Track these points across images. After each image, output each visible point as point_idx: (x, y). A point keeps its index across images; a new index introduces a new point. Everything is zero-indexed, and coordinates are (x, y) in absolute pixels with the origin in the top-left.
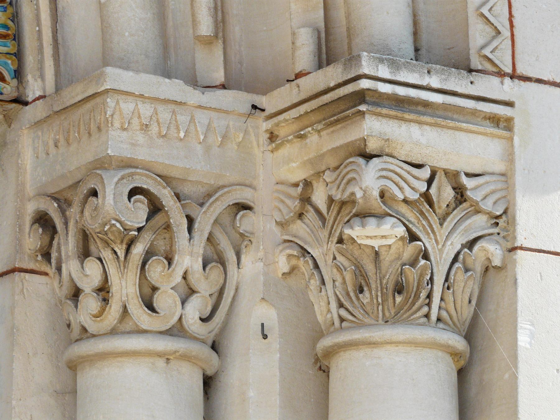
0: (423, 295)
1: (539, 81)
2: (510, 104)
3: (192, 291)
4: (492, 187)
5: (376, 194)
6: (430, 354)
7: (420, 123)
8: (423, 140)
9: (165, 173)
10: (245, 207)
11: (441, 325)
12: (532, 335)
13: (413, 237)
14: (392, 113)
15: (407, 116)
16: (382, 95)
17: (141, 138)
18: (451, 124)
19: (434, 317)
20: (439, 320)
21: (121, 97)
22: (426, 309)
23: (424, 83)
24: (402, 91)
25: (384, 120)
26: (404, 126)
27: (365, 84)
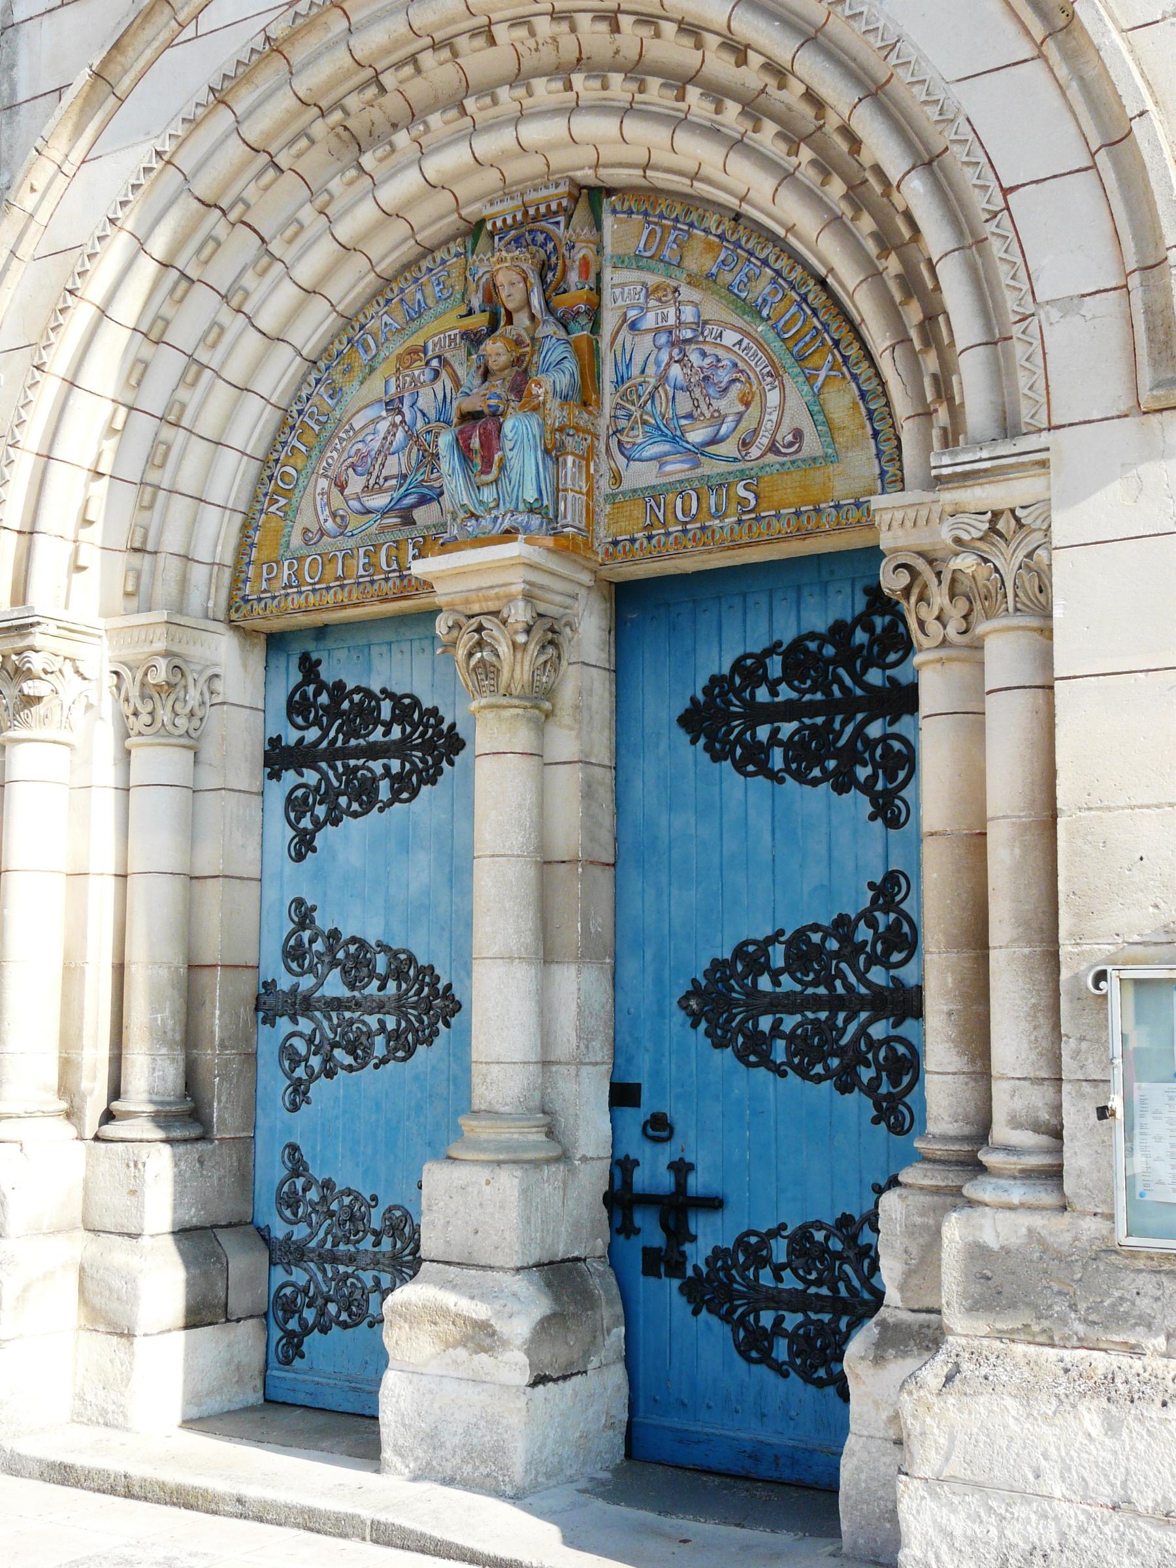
0: (999, 597)
1: (1071, 425)
2: (1047, 449)
3: (938, 618)
4: (1040, 511)
5: (949, 541)
6: (1012, 636)
7: (981, 484)
8: (984, 495)
9: (919, 549)
10: (217, 676)
11: (1018, 613)
12: (1065, 608)
13: (986, 561)
14: (956, 485)
15: (980, 481)
16: (949, 475)
17: (900, 532)
18: (1001, 478)
19: (1011, 609)
20: (1017, 610)
21: (883, 512)
22: (1004, 606)
23: (977, 458)
24: (959, 469)
25: (954, 491)
26: (969, 490)
27: (934, 472)
